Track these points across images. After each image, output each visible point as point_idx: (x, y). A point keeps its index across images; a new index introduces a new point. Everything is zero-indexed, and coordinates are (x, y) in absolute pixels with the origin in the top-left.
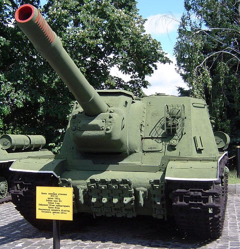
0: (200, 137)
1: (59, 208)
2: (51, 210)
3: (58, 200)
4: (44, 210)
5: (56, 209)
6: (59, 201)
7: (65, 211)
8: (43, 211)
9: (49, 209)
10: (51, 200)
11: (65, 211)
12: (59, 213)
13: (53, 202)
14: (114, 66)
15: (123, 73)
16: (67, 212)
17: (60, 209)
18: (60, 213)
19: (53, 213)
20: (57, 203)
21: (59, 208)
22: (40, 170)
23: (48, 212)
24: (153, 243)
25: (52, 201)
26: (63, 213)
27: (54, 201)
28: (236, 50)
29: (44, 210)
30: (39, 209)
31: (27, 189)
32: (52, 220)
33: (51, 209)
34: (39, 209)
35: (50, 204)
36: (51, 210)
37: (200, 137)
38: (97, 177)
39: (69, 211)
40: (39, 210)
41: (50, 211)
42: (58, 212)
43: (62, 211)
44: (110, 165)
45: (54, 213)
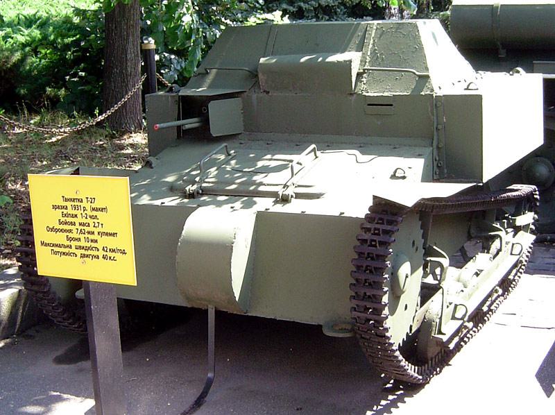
1: (96, 241)
2: (73, 247)
4: (57, 245)
5: (88, 245)
7: (114, 251)
9: (68, 243)
11: (114, 251)
12: (98, 257)
14: (405, 402)
16: (118, 256)
17: (99, 245)
18: (101, 257)
19: (83, 256)
21: (96, 241)
24: (480, 8)
29: (57, 245)
30: (42, 243)
31: (187, 189)
32: (81, 280)
33: (73, 244)
34: (42, 243)
35: (83, 228)
36: (73, 247)
38: (74, 38)
39: (124, 252)
40: (43, 247)
41: (73, 250)
42: (95, 253)
43: (103, 250)
44: (410, 206)
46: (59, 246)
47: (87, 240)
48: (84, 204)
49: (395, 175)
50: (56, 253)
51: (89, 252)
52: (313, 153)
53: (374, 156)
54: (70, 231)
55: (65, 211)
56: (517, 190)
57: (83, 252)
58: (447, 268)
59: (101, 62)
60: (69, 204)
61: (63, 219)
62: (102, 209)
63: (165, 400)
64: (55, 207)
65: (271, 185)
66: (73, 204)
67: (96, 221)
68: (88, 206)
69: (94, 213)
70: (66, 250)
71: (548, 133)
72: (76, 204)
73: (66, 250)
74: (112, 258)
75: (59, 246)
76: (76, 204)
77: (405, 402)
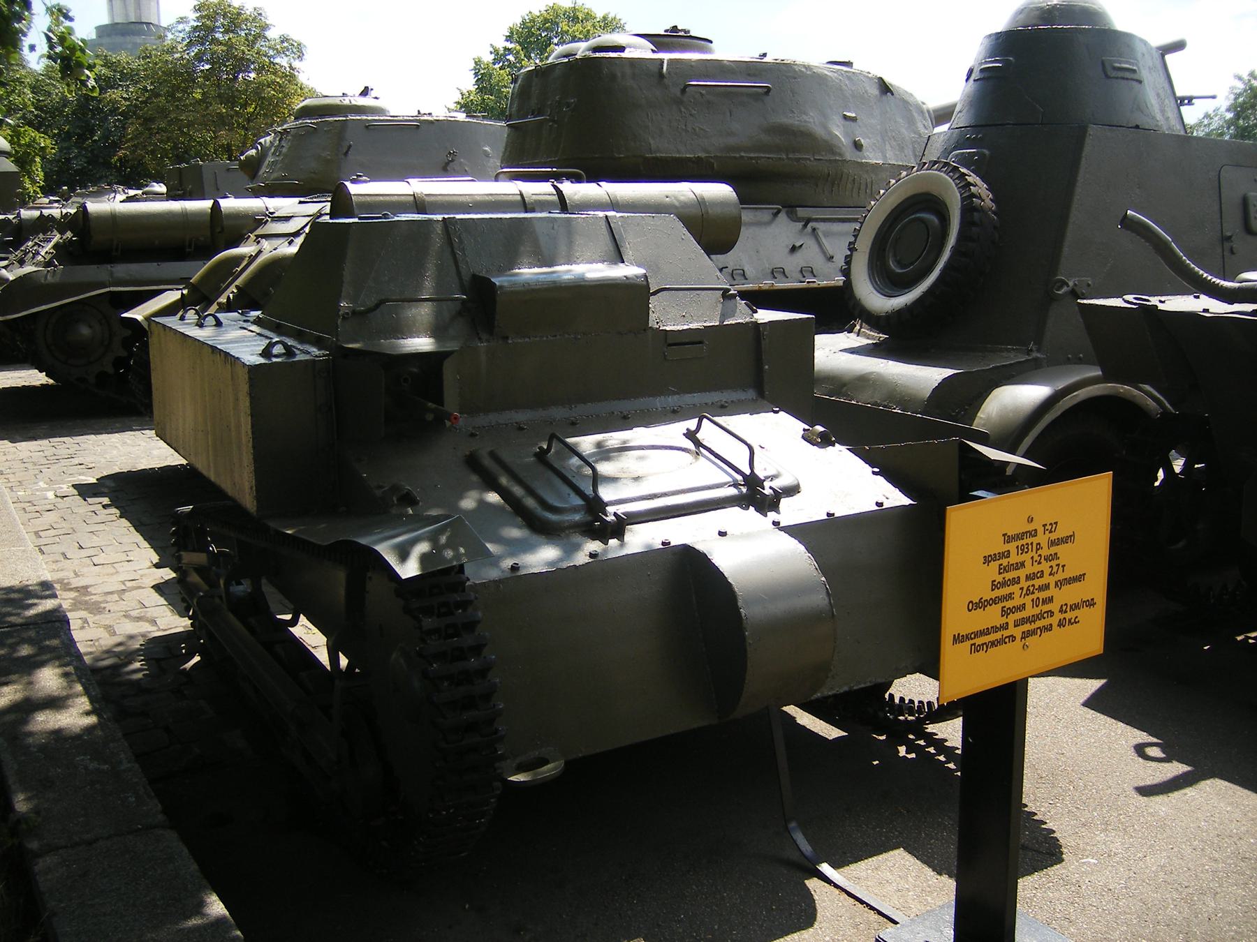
8: (979, 641)
11: (1076, 607)
47: (1036, 603)
48: (1042, 538)
49: (1182, 104)
50: (976, 649)
51: (1039, 624)
53: (1155, 740)
54: (1010, 596)
55: (1005, 562)
56: (852, 351)
57: (1027, 627)
59: (134, 346)
60: (1012, 547)
61: (999, 579)
63: (1229, 857)
64: (988, 560)
65: (993, 644)
66: (1020, 543)
67: (1054, 563)
68: (1042, 538)
69: (1053, 550)
72: (1024, 542)
76: (1024, 542)
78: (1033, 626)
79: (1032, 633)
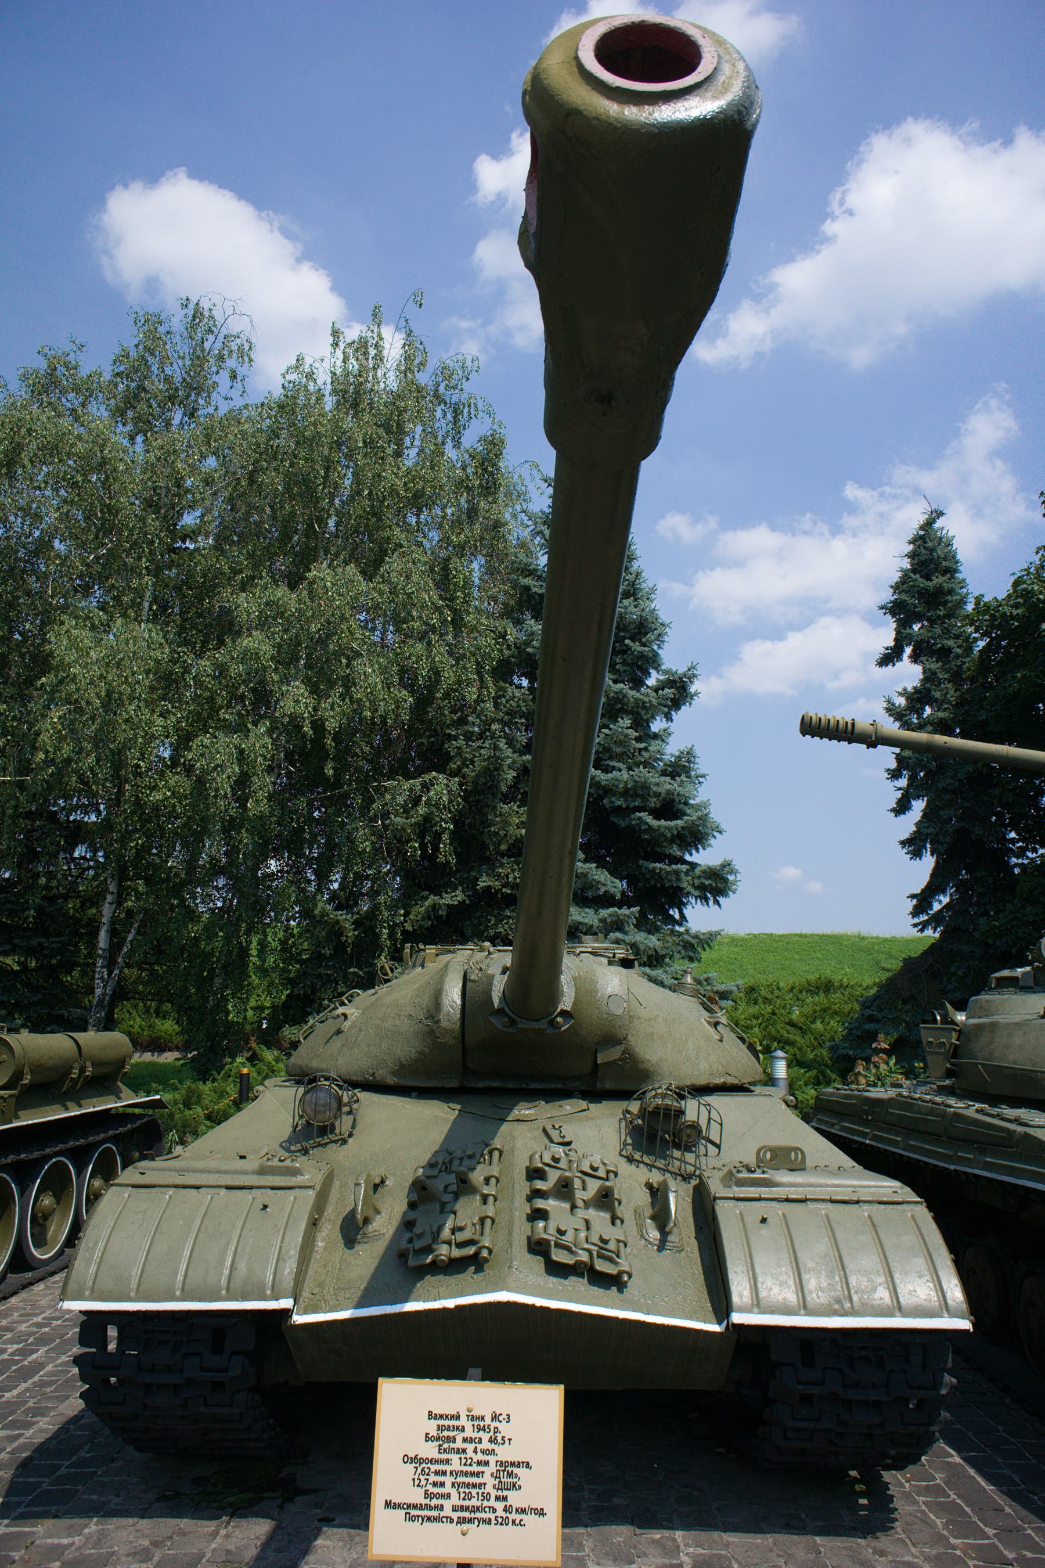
0: (811, 728)
3: (485, 1437)
4: (435, 1519)
6: (490, 1441)
7: (524, 1511)
8: (414, 1512)
10: (440, 1502)
11: (524, 1511)
13: (459, 1444)
15: (717, 902)
16: (529, 1519)
19: (462, 1521)
20: (483, 1452)
22: (359, 1305)
23: (436, 1519)
25: (442, 1508)
26: (505, 1522)
27: (465, 1440)
28: (874, 1138)
29: (435, 1519)
30: (388, 1504)
34: (388, 1504)
37: (811, 728)
39: (541, 1513)
40: (389, 1511)
41: (448, 1511)
45: (465, 1527)
46: (415, 1507)
50: (412, 1519)
51: (478, 1515)
52: (763, 1077)
58: (666, 672)
62: (519, 1463)
69: (445, 1456)
70: (434, 1513)
71: (639, 465)
73: (434, 1513)
74: (517, 1522)
75: (415, 1507)
77: (696, 694)
78: (473, 1515)
79: (470, 1521)
